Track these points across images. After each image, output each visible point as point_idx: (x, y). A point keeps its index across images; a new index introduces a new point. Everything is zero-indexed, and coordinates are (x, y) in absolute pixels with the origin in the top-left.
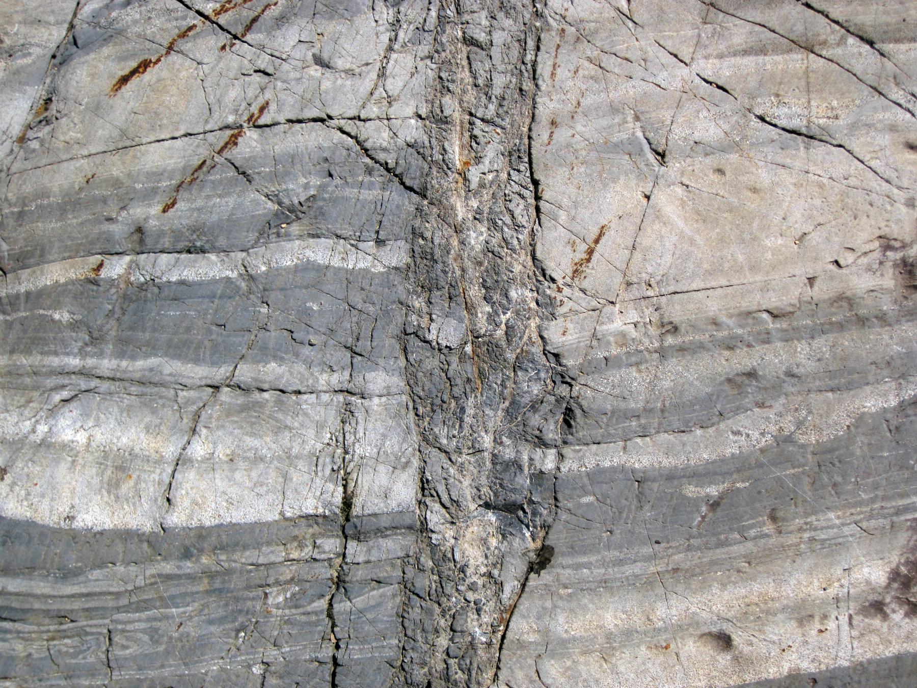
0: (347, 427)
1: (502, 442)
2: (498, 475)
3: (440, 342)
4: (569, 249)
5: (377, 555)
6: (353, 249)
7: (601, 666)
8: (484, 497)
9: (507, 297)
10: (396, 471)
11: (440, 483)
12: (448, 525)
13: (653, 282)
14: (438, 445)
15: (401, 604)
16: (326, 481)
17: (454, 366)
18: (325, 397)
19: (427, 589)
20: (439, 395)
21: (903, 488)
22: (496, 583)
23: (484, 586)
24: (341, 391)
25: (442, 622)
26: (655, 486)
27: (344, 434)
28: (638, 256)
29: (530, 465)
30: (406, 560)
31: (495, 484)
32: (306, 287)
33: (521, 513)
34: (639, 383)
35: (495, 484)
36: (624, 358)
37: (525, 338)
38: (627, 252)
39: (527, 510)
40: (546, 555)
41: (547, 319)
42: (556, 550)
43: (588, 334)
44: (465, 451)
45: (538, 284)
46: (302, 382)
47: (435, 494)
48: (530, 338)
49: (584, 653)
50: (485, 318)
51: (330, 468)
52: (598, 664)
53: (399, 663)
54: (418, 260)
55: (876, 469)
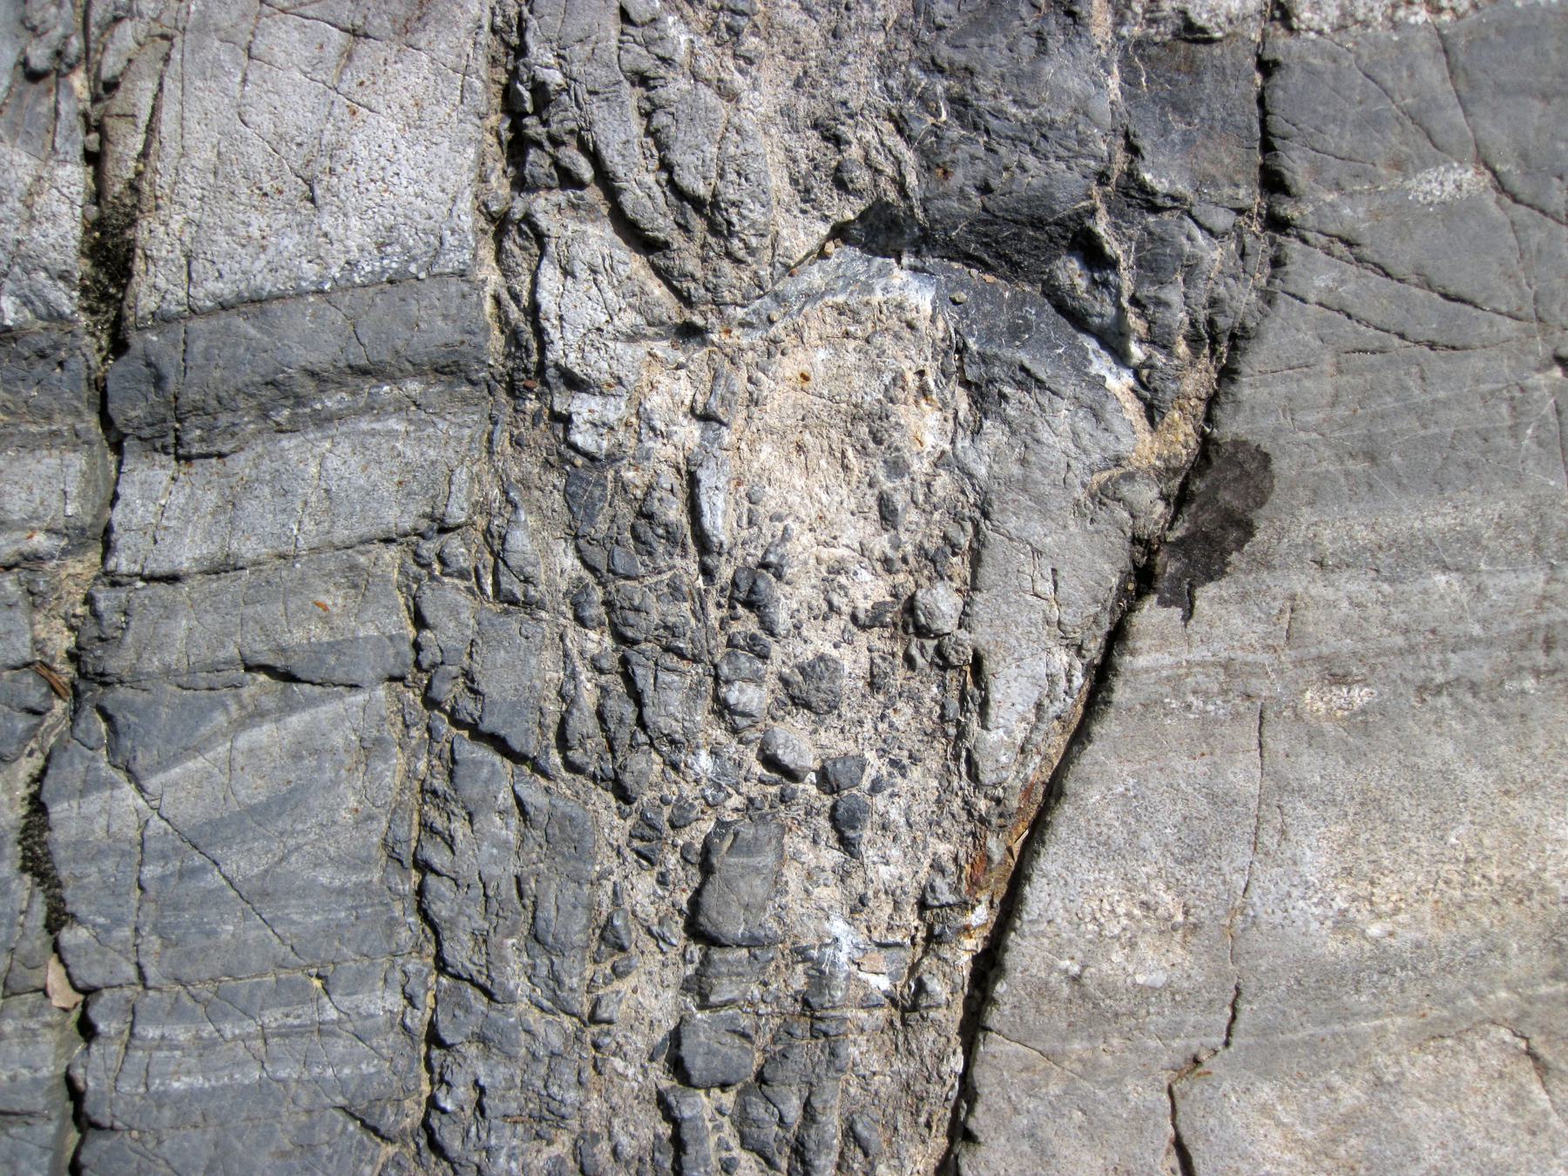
2: (944, 52)
5: (269, 523)
7: (1519, 1101)
8: (862, 178)
10: (364, 48)
12: (661, 348)
15: (411, 798)
19: (553, 708)
22: (942, 661)
23: (874, 683)
25: (642, 889)
30: (428, 548)
33: (1071, 272)
39: (1113, 248)
40: (1226, 497)
42: (1280, 465)
47: (586, 171)
49: (1430, 1035)
52: (1502, 1094)
53: (414, 1112)
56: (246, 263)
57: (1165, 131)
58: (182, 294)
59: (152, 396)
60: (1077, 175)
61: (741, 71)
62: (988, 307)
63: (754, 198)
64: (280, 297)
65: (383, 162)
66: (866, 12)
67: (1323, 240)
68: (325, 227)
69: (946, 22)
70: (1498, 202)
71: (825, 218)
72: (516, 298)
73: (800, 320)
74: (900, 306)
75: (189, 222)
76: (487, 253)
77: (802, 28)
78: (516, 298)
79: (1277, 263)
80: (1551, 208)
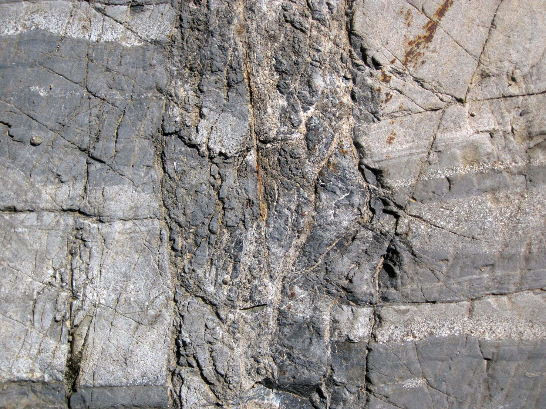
0: (77, 262)
1: (293, 295)
2: (286, 342)
3: (212, 146)
4: (401, 22)
6: (99, 15)
8: (263, 372)
9: (310, 86)
10: (141, 327)
11: (202, 348)
13: (518, 75)
14: (202, 294)
16: (45, 336)
17: (229, 181)
18: (49, 218)
20: (207, 222)
24: (71, 210)
26: (512, 367)
27: (72, 270)
28: (498, 36)
29: (333, 330)
31: (281, 353)
32: (32, 65)
33: (316, 397)
34: (495, 217)
35: (281, 353)
36: (475, 180)
37: (334, 145)
38: (484, 31)
39: (326, 394)
41: (366, 119)
43: (426, 143)
44: (240, 303)
45: (355, 70)
46: (18, 196)
47: (194, 364)
48: (340, 146)
50: (277, 115)
51: (51, 317)
54: (187, 32)
56: (108, 377)
57: (341, 365)
58: (92, 382)
59: (82, 404)
60: (317, 375)
61: (235, 343)
62: (294, 404)
63: (236, 375)
64: (117, 386)
65: (144, 356)
66: (267, 330)
67: (380, 396)
68: (129, 371)
69: (287, 334)
70: (427, 388)
71: (254, 380)
72: (176, 392)
73: (246, 405)
74: (271, 405)
75: (94, 364)
76: (169, 380)
77: (251, 333)
78: (176, 392)
79: (368, 401)
80: (441, 390)
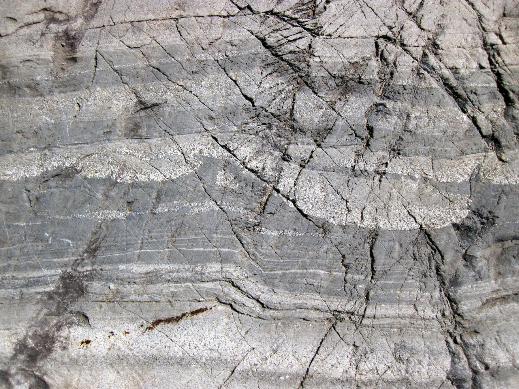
21: (36, 260)
55: (11, 238)
